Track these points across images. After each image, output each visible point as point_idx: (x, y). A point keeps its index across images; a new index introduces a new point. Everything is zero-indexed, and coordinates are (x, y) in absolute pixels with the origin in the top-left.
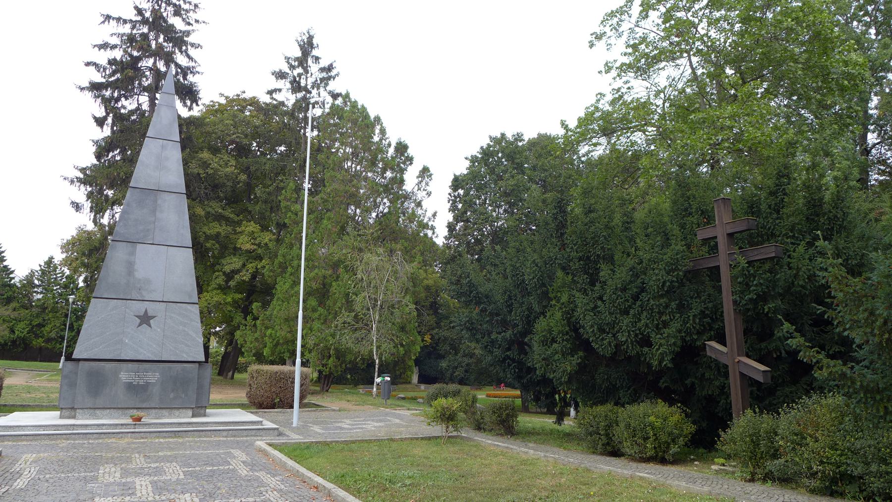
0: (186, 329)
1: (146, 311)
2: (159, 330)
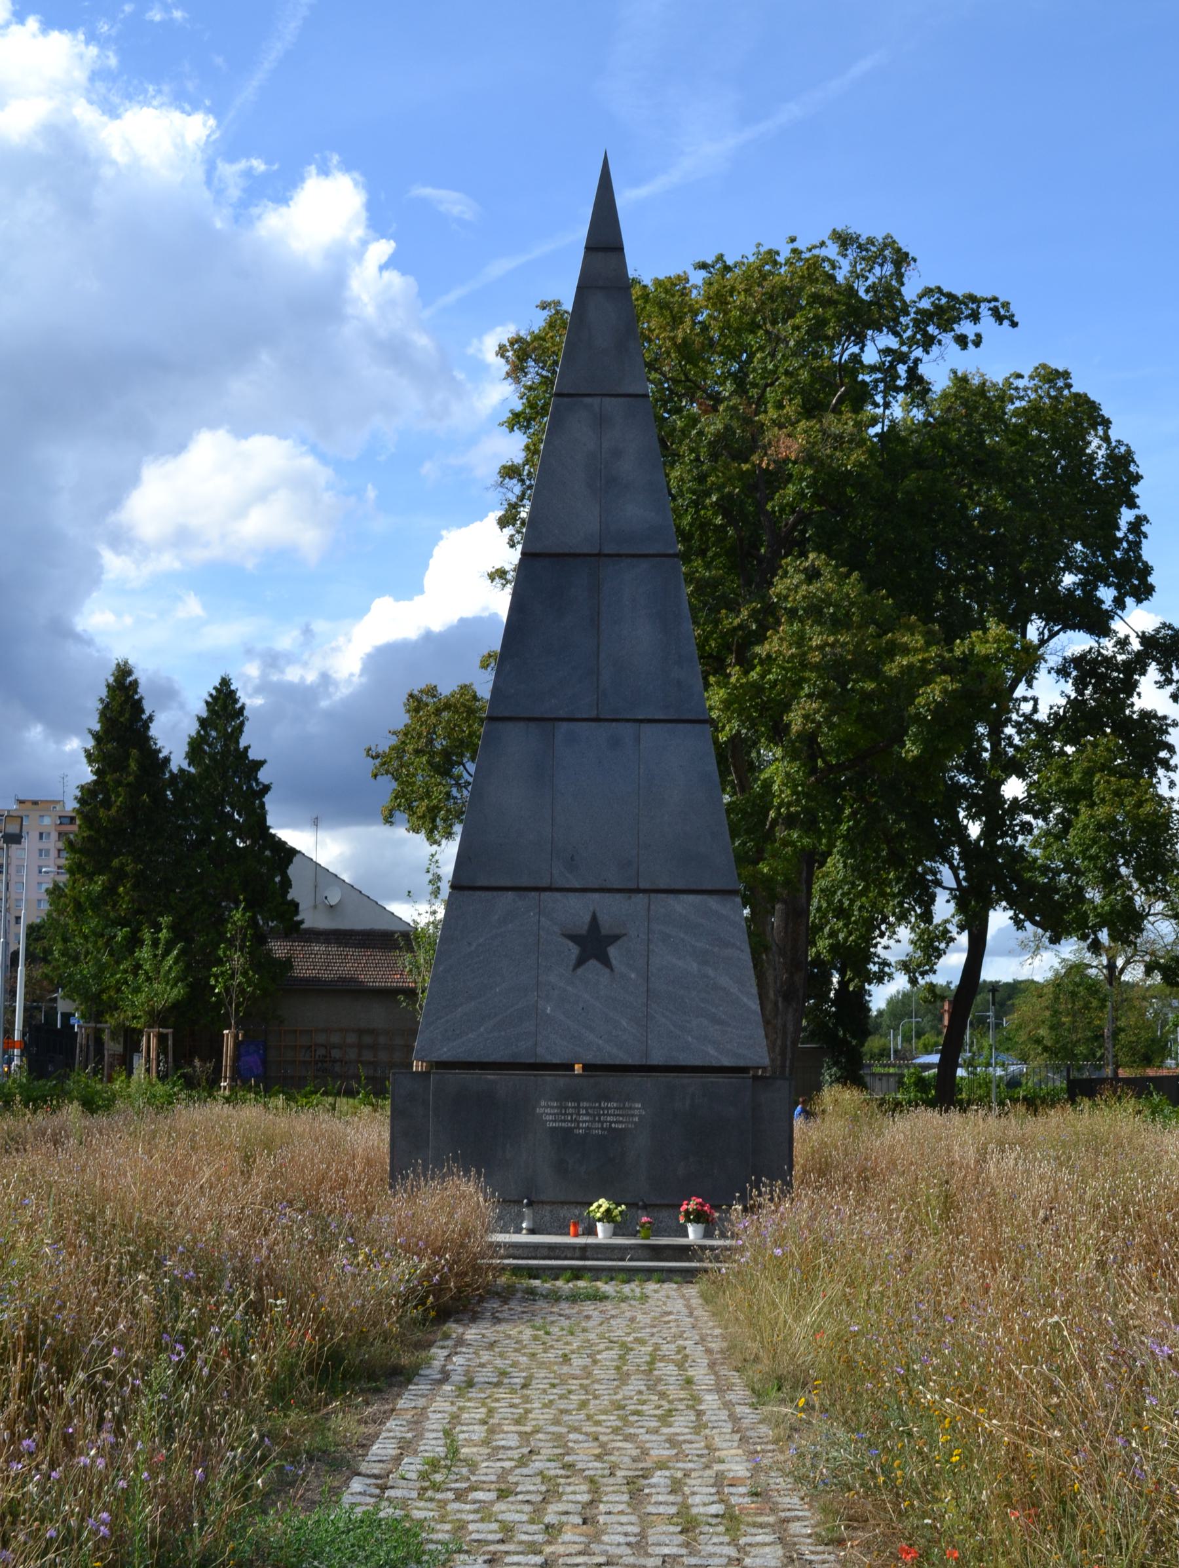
0: (711, 972)
1: (594, 918)
2: (633, 976)
